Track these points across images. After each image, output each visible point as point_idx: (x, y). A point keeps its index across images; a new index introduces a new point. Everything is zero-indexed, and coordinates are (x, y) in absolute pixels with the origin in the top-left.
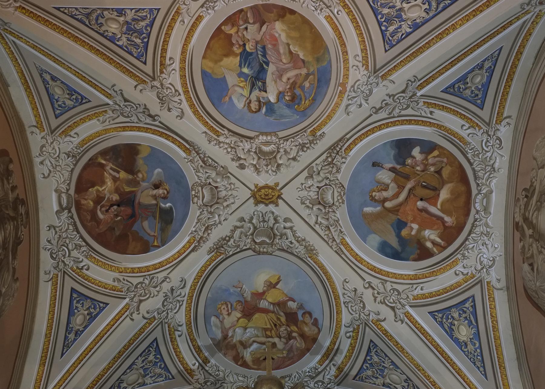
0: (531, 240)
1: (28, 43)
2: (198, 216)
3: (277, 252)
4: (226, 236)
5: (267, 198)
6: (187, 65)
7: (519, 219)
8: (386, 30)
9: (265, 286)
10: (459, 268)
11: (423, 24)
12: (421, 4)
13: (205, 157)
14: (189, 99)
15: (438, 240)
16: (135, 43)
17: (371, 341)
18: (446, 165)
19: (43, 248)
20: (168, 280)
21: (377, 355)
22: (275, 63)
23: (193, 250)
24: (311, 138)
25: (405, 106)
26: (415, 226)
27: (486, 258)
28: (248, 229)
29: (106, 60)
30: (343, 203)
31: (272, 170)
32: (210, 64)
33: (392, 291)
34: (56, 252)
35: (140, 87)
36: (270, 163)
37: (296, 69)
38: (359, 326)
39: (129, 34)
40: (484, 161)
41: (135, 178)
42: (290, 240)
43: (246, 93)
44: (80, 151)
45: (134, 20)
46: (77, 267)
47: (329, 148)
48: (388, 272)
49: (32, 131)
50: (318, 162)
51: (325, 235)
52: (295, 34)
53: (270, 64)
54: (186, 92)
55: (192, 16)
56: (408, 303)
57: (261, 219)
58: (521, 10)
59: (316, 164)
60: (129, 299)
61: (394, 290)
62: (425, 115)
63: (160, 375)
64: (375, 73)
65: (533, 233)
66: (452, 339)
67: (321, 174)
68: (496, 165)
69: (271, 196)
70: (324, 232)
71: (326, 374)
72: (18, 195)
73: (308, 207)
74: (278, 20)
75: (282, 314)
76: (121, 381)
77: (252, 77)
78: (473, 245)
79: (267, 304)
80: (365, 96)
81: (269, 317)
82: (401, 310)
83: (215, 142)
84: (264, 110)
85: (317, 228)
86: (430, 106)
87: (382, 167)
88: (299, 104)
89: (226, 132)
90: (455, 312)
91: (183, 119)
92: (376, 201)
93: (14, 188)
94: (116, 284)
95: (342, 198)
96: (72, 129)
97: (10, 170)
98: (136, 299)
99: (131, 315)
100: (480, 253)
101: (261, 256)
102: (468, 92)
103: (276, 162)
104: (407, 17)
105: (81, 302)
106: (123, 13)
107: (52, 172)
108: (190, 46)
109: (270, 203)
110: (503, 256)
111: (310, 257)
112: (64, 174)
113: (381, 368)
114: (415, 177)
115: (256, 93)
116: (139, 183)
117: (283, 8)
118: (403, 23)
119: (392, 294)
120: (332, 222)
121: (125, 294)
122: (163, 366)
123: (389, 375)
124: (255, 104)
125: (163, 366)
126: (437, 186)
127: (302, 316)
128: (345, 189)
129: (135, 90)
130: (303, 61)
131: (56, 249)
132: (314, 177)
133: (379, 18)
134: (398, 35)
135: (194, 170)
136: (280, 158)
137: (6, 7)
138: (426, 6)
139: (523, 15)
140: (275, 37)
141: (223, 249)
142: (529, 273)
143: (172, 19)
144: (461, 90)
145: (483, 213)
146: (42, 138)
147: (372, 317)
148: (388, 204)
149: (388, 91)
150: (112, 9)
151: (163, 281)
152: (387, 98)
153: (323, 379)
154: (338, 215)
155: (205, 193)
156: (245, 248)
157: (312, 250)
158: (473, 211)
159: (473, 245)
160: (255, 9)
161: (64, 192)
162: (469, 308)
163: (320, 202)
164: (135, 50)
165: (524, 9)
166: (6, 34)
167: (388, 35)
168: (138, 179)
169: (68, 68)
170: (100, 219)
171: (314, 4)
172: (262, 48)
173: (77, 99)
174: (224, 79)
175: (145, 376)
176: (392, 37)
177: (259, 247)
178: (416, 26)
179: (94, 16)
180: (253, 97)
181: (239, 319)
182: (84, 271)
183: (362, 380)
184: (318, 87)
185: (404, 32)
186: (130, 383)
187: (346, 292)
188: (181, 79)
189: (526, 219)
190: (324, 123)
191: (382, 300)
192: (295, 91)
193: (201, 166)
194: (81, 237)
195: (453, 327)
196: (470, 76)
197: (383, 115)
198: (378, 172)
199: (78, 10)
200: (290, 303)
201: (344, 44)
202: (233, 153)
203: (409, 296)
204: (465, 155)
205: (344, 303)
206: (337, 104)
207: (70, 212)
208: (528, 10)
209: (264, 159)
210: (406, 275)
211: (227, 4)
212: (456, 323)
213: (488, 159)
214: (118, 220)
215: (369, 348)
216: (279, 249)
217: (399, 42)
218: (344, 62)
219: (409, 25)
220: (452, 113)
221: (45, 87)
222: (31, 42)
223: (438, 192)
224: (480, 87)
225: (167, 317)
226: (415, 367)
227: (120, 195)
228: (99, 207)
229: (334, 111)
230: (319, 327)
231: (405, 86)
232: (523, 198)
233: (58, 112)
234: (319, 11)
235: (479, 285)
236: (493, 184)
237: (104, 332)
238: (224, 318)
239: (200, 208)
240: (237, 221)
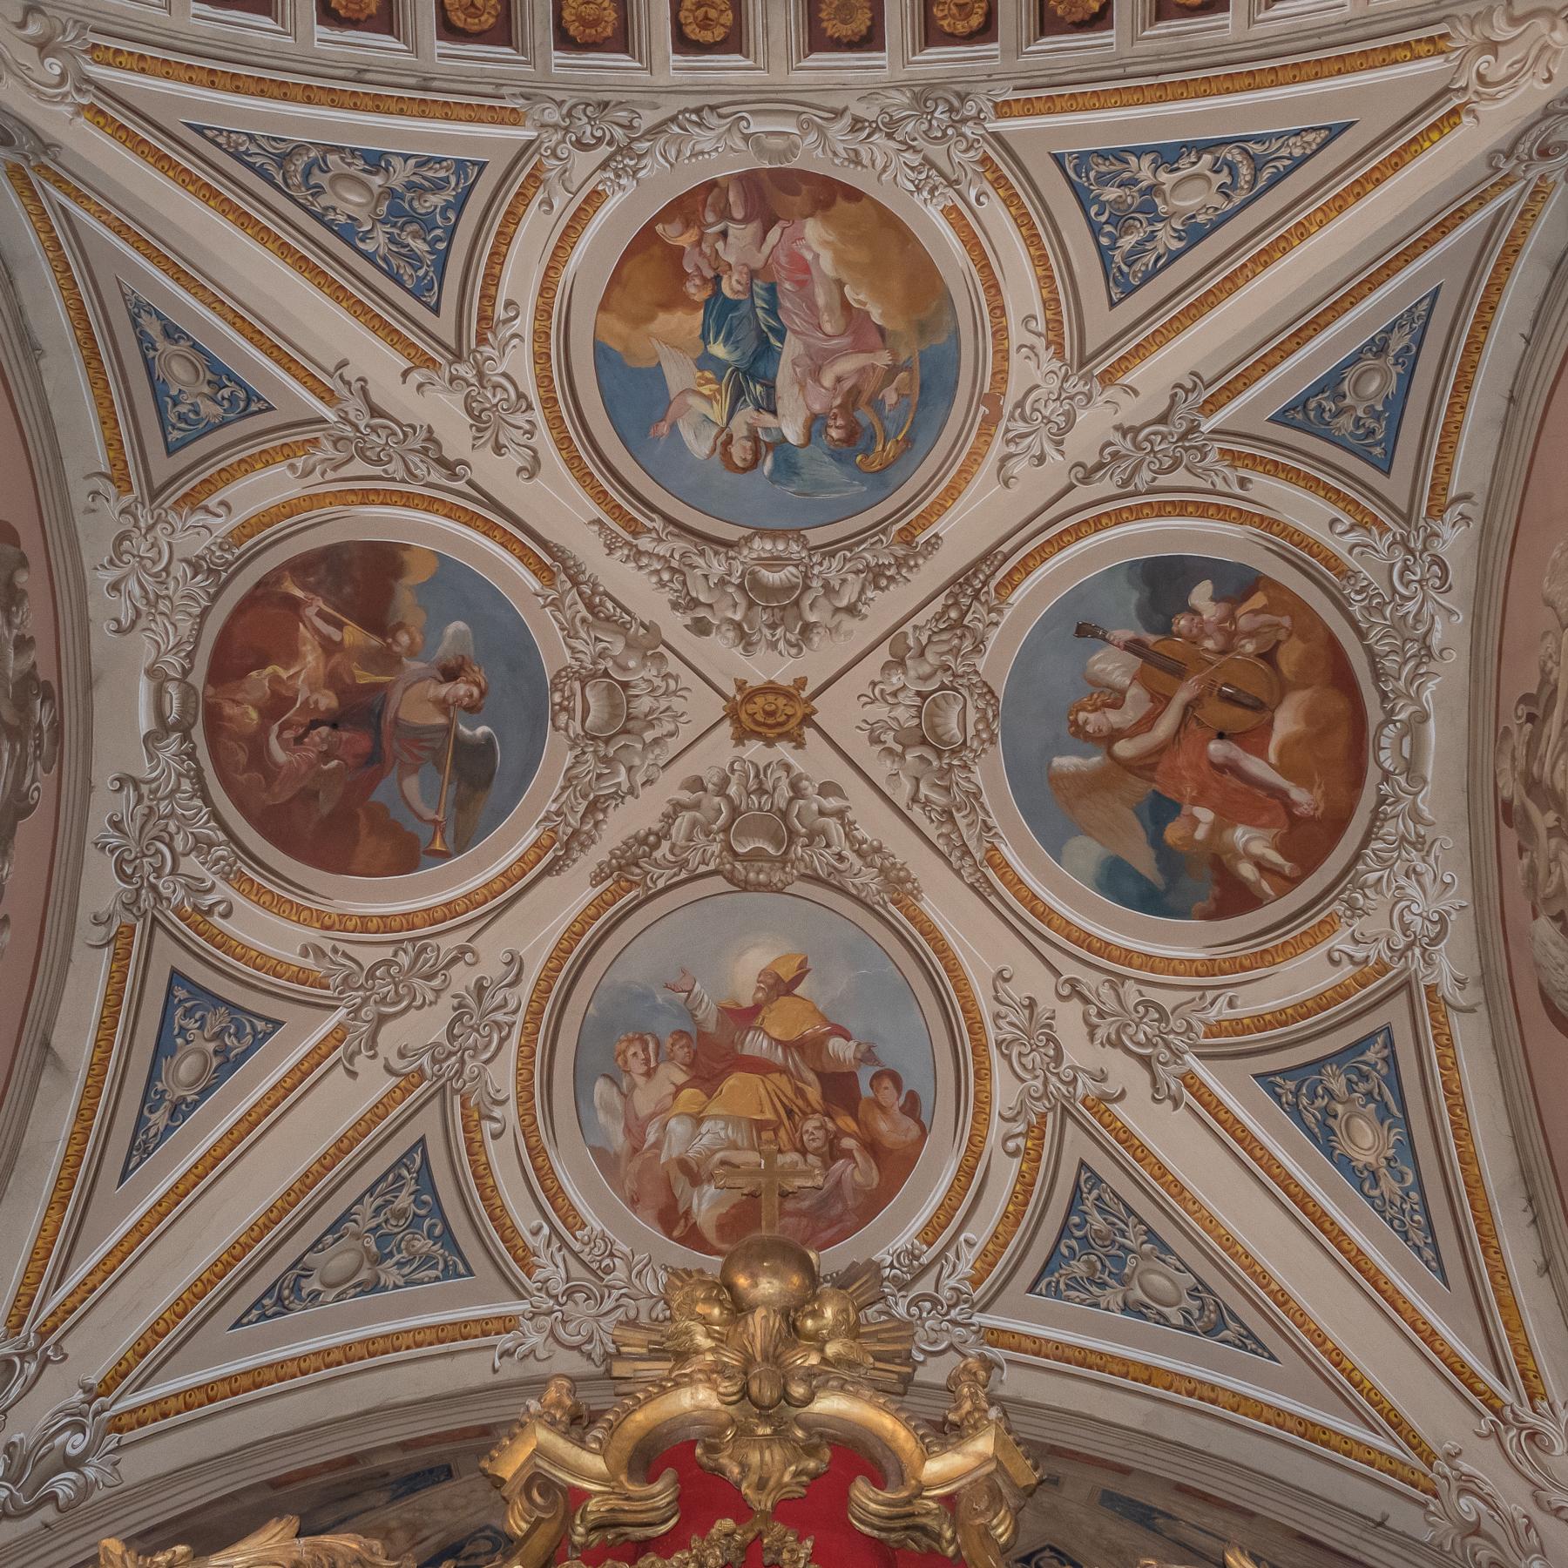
0: (1554, 842)
1: (104, 217)
2: (568, 769)
3: (797, 883)
4: (650, 833)
5: (770, 721)
6: (554, 326)
7: (1511, 788)
8: (1113, 247)
9: (759, 989)
10: (1339, 941)
11: (1217, 225)
12: (1208, 173)
13: (594, 593)
14: (555, 422)
15: (1275, 857)
16: (412, 250)
17: (1082, 1164)
18: (1290, 635)
19: (97, 844)
20: (468, 957)
21: (1101, 1210)
22: (802, 333)
23: (547, 871)
24: (900, 551)
25: (1168, 462)
27: (1420, 915)
28: (712, 814)
29: (325, 289)
30: (992, 743)
31: (788, 642)
32: (619, 327)
33: (1141, 1009)
34: (136, 858)
35: (416, 377)
36: (782, 619)
38: (1044, 1116)
39: (394, 225)
40: (1398, 626)
41: (389, 646)
42: (835, 849)
43: (718, 413)
44: (229, 557)
45: (411, 186)
46: (196, 908)
47: (953, 581)
48: (1129, 951)
49: (95, 488)
50: (919, 619)
51: (939, 836)
52: (859, 255)
54: (549, 402)
55: (574, 190)
56: (1190, 1046)
57: (753, 785)
58: (1489, 172)
59: (915, 627)
60: (345, 1011)
61: (1148, 1004)
62: (1226, 489)
63: (428, 1260)
64: (1082, 365)
65: (1558, 820)
66: (1330, 1157)
67: (931, 657)
68: (1436, 640)
69: (784, 718)
70: (937, 828)
71: (946, 1273)
72: (34, 665)
73: (890, 751)
74: (811, 215)
75: (811, 1077)
76: (303, 1269)
77: (737, 369)
78: (1379, 874)
79: (765, 1044)
80: (1054, 431)
81: (770, 1087)
83: (626, 552)
84: (768, 465)
85: (916, 814)
86: (1238, 463)
87: (1105, 640)
88: (867, 452)
89: (658, 524)
90: (1334, 1074)
91: (536, 480)
92: (1088, 737)
93: (23, 644)
94: (309, 962)
95: (988, 726)
96: (212, 488)
97: (19, 586)
98: (368, 1012)
99: (351, 1059)
100: (1400, 900)
102: (1346, 422)
103: (800, 617)
104: (1172, 210)
105: (197, 1016)
106: (383, 164)
107: (144, 615)
108: (567, 273)
109: (781, 736)
110: (1471, 911)
111: (895, 903)
112: (179, 625)
113: (1113, 1252)
114: (1201, 671)
116: (399, 662)
117: (828, 182)
118: (1160, 225)
119: (1142, 1018)
120: (960, 797)
121: (336, 995)
122: (437, 1231)
123: (1142, 1273)
124: (744, 448)
125: (437, 1231)
126: (1265, 698)
127: (871, 1086)
128: (998, 701)
129: (404, 382)
130: (881, 330)
131: (135, 851)
132: (909, 663)
133: (1092, 214)
134: (1145, 260)
135: (562, 629)
136: (812, 606)
137: (51, 100)
138: (1224, 178)
139: (1496, 189)
140: (803, 258)
141: (637, 871)
142: (1555, 944)
143: (518, 194)
144: (1327, 416)
145: (1402, 780)
146: (122, 512)
147: (1084, 1086)
148: (1124, 748)
149: (1117, 419)
150: (353, 151)
151: (454, 961)
152: (1116, 437)
153: (937, 1291)
154: (978, 777)
155: (591, 700)
156: (702, 869)
157: (902, 881)
158: (1373, 774)
159: (1378, 874)
160: (750, 182)
161: (174, 679)
162: (1376, 1063)
163: (926, 737)
164: (409, 271)
165: (1498, 169)
166: (47, 186)
167: (1118, 259)
168: (396, 649)
169: (214, 303)
170: (276, 764)
171: (912, 175)
172: (766, 290)
173: (232, 399)
174: (657, 373)
175: (379, 1260)
176: (1129, 266)
177: (745, 868)
178: (1195, 234)
179: (300, 163)
180: (739, 426)
181: (679, 1089)
182: (216, 920)
183: (1057, 1294)
184: (922, 404)
185: (1161, 250)
186: (330, 1278)
187: (1003, 1010)
188: (536, 363)
189: (1533, 785)
190: (939, 509)
191: (1113, 1036)
192: (857, 414)
193: (584, 620)
194: (215, 815)
195: (1331, 1122)
196: (1351, 374)
197: (1105, 486)
198: (1093, 653)
199: (255, 140)
200: (836, 1044)
201: (996, 286)
202: (677, 586)
203: (1194, 1023)
204: (1342, 606)
205: (999, 1044)
206: (975, 453)
207: (186, 737)
208: (1507, 175)
209: (765, 608)
210: (1181, 961)
211: (672, 165)
212: (1340, 1108)
213: (1410, 620)
214: (329, 770)
215: (1077, 1186)
216: (804, 875)
217: (1148, 277)
218: (994, 334)
219: (1175, 230)
220: (1303, 484)
221: (145, 357)
222: (115, 213)
223: (1267, 716)
224: (1379, 408)
225: (459, 1073)
226: (1220, 1245)
227: (340, 694)
228: (275, 728)
229: (966, 474)
230: (922, 1118)
231: (1167, 402)
232: (1521, 726)
233: (175, 435)
234: (925, 194)
235: (1403, 996)
237: (260, 1110)
238: (633, 1086)
240: (681, 788)
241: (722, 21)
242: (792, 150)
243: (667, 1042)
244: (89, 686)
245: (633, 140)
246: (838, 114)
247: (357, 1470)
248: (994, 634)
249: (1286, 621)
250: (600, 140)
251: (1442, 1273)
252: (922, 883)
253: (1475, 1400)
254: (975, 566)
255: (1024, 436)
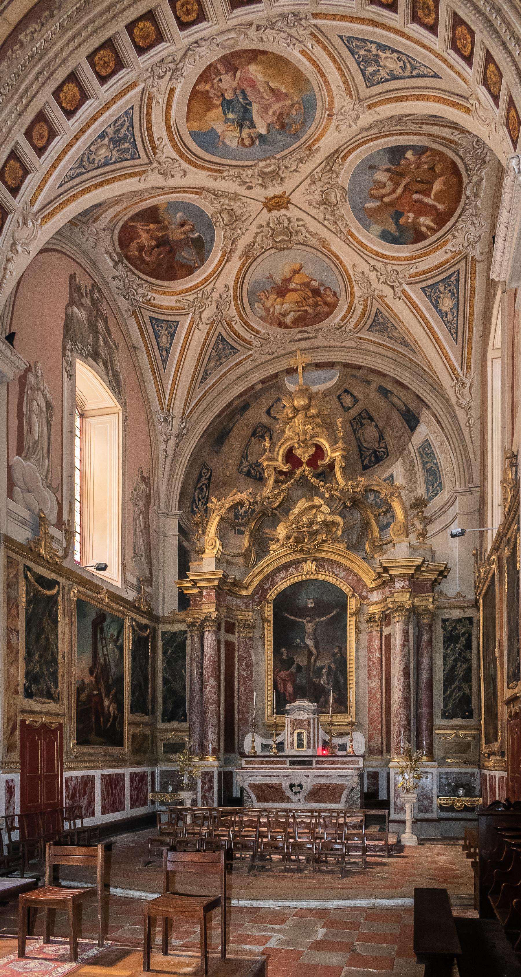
10: (449, 247)
15: (432, 224)
23: (227, 261)
26: (411, 215)
32: (196, 124)
35: (143, 178)
37: (280, 101)
43: (237, 133)
45: (115, 132)
47: (327, 158)
50: (318, 170)
53: (253, 104)
54: (182, 155)
57: (277, 222)
61: (394, 270)
63: (230, 353)
67: (323, 179)
68: (487, 159)
73: (315, 207)
74: (250, 63)
77: (238, 120)
82: (399, 288)
84: (257, 142)
85: (326, 223)
89: (228, 168)
94: (178, 304)
95: (344, 198)
98: (197, 312)
101: (282, 252)
103: (279, 176)
108: (172, 119)
109: (282, 208)
115: (246, 132)
126: (430, 180)
130: (286, 94)
145: (473, 198)
147: (377, 293)
148: (386, 200)
151: (212, 292)
154: (343, 211)
158: (464, 198)
160: (224, 60)
163: (325, 202)
174: (213, 130)
176: (372, 77)
180: (245, 134)
181: (275, 299)
182: (152, 301)
190: (318, 140)
192: (284, 120)
194: (139, 278)
200: (313, 283)
201: (325, 75)
204: (456, 153)
207: (123, 263)
212: (441, 295)
215: (376, 313)
217: (379, 83)
225: (222, 316)
227: (156, 240)
229: (325, 130)
236: (483, 174)
238: (264, 302)
239: (223, 229)
241: (194, 9)
242: (236, 44)
243: (270, 290)
244: (94, 263)
245: (177, 65)
246: (250, 25)
247: (231, 408)
248: (342, 172)
249: (438, 158)
250: (166, 72)
251: (456, 341)
252: (330, 241)
253: (453, 376)
254: (333, 154)
255: (343, 120)
